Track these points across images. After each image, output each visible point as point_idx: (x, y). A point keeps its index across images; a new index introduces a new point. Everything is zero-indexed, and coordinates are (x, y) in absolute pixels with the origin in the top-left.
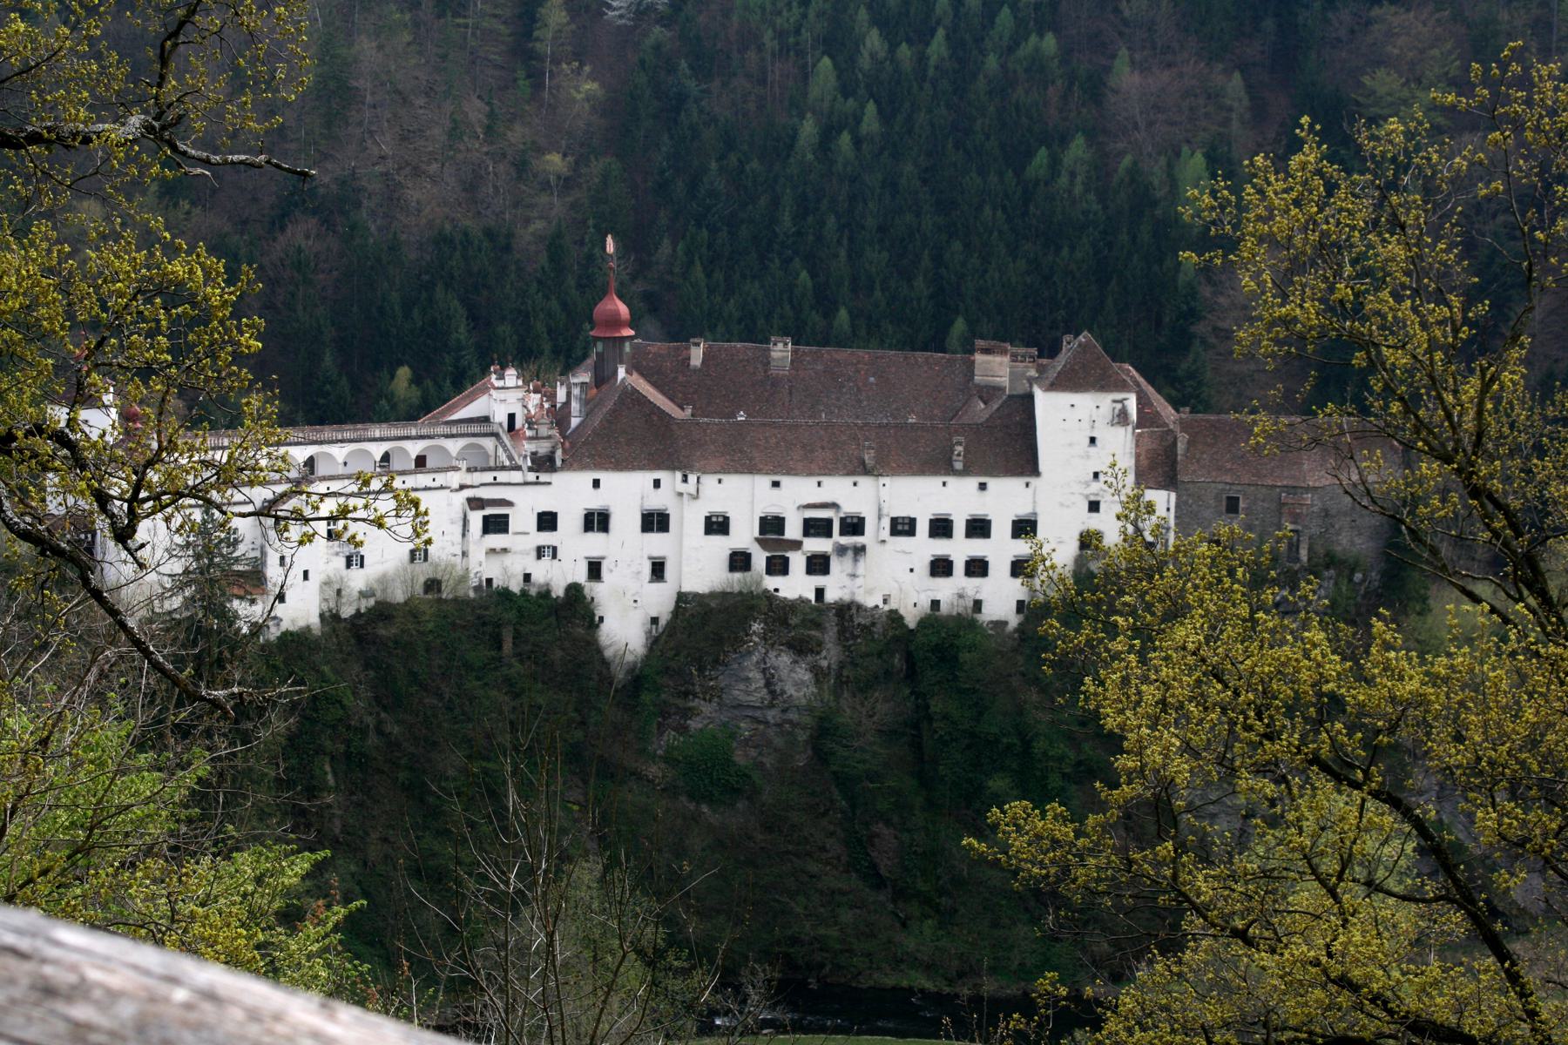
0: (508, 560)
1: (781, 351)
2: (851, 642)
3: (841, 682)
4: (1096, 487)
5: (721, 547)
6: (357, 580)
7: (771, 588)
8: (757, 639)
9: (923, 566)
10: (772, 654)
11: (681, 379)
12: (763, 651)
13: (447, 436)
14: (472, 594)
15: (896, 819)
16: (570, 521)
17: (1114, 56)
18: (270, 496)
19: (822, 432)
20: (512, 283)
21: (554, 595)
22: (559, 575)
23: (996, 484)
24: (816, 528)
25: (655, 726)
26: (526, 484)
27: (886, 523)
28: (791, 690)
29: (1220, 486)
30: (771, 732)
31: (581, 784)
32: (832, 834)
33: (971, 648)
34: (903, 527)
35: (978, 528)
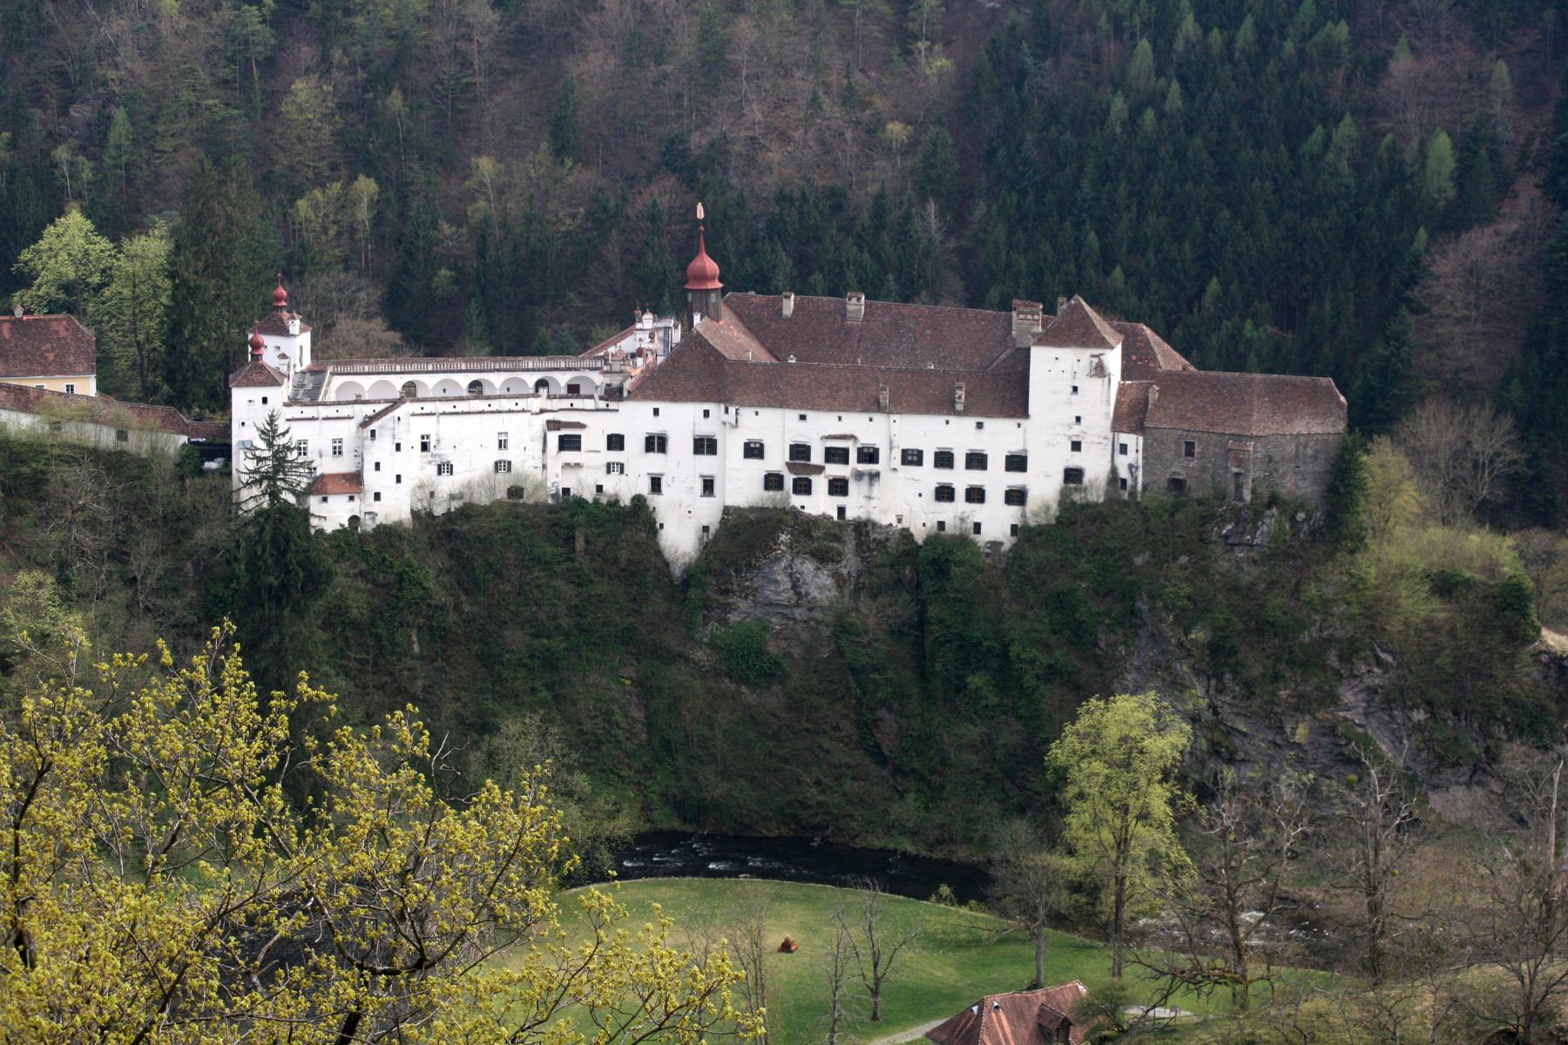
0: (582, 473)
1: (857, 305)
3: (858, 589)
4: (1077, 429)
5: (758, 468)
6: (446, 485)
8: (784, 548)
9: (930, 493)
11: (774, 325)
13: (591, 369)
14: (550, 501)
15: (896, 706)
16: (634, 443)
17: (1395, 42)
18: (371, 413)
19: (849, 375)
20: (832, 237)
22: (625, 488)
23: (991, 424)
24: (836, 455)
25: (701, 617)
26: (598, 410)
27: (898, 455)
28: (814, 593)
29: (1180, 432)
30: (799, 628)
31: (635, 662)
32: (847, 716)
33: (960, 563)
34: (912, 458)
35: (977, 461)
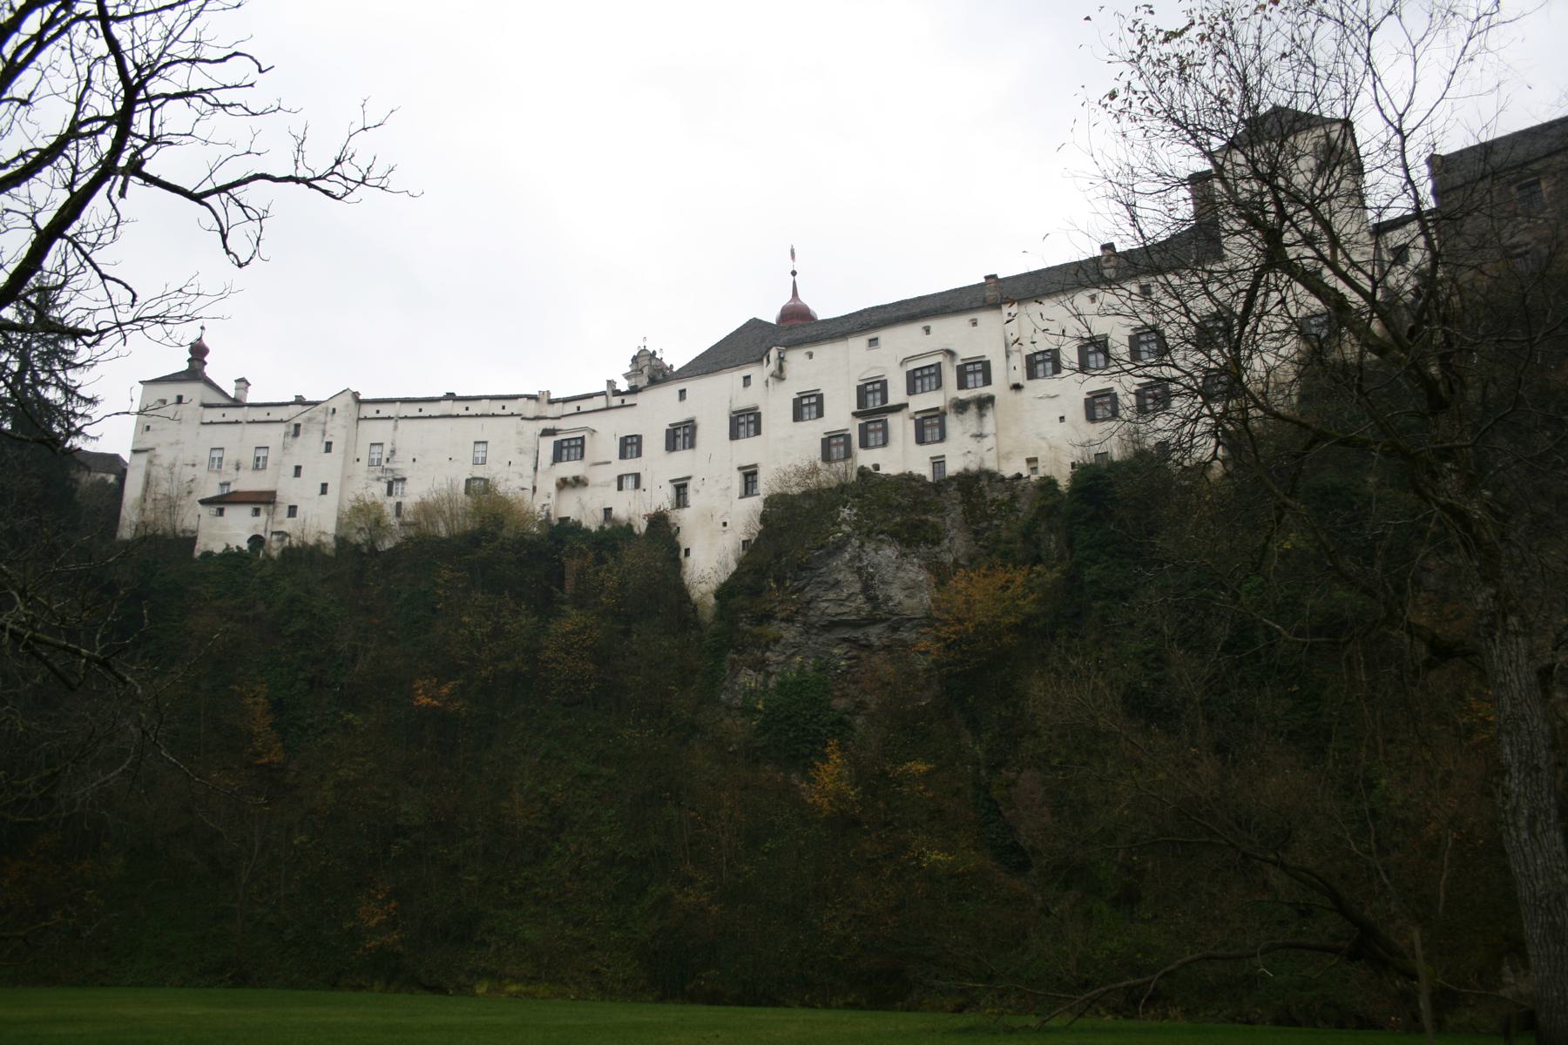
0: (585, 495)
2: (985, 524)
5: (812, 433)
7: (869, 464)
9: (1077, 411)
10: (870, 547)
12: (857, 543)
21: (636, 530)
26: (608, 408)
27: (1018, 361)
28: (897, 594)
34: (1043, 363)
